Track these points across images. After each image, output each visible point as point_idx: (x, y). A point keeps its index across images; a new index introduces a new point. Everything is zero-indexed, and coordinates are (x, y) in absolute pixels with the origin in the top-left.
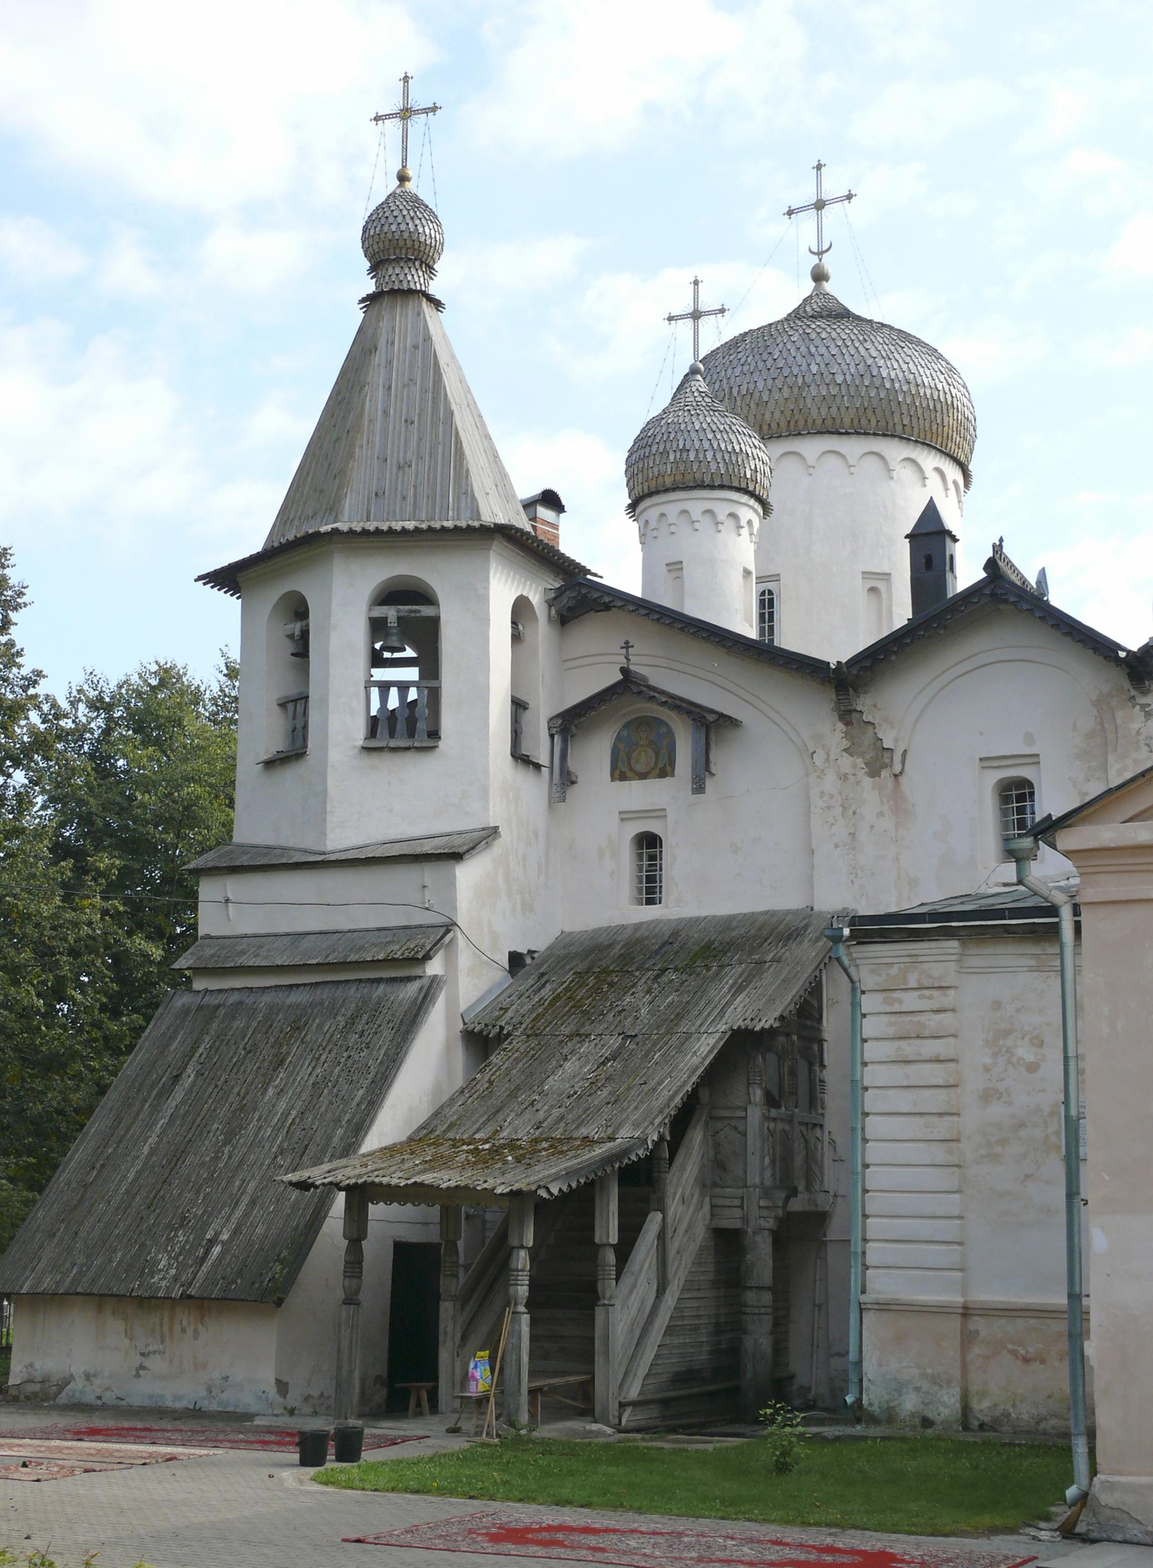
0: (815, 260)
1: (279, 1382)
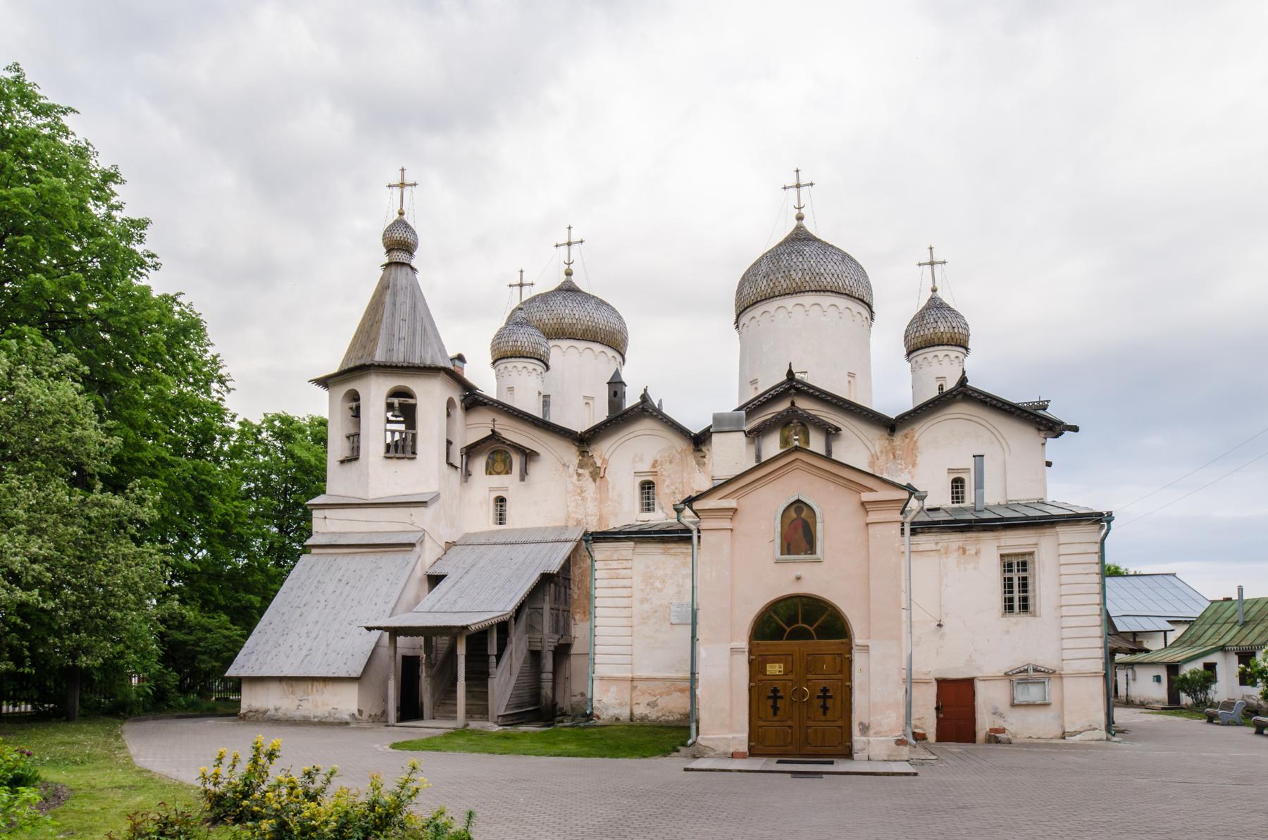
0: (566, 267)
1: (359, 710)
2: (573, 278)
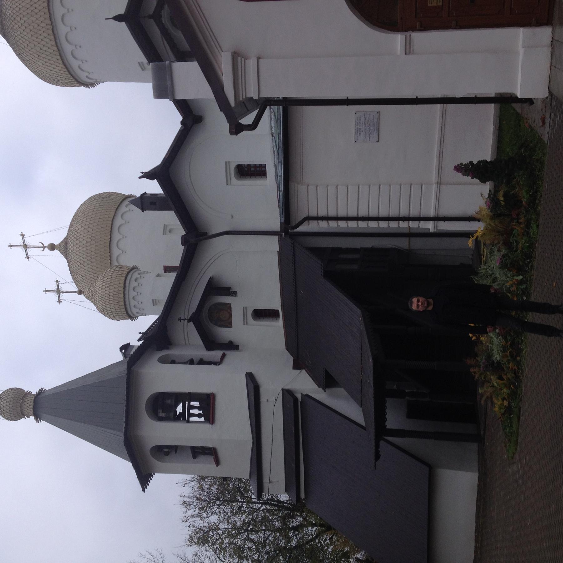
0: (46, 249)
2: (56, 243)
